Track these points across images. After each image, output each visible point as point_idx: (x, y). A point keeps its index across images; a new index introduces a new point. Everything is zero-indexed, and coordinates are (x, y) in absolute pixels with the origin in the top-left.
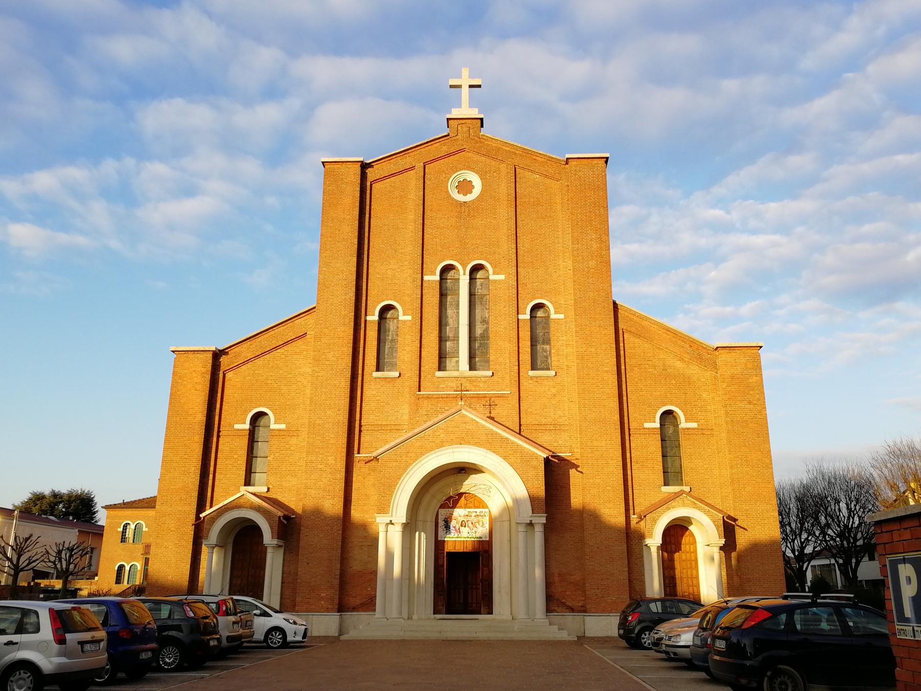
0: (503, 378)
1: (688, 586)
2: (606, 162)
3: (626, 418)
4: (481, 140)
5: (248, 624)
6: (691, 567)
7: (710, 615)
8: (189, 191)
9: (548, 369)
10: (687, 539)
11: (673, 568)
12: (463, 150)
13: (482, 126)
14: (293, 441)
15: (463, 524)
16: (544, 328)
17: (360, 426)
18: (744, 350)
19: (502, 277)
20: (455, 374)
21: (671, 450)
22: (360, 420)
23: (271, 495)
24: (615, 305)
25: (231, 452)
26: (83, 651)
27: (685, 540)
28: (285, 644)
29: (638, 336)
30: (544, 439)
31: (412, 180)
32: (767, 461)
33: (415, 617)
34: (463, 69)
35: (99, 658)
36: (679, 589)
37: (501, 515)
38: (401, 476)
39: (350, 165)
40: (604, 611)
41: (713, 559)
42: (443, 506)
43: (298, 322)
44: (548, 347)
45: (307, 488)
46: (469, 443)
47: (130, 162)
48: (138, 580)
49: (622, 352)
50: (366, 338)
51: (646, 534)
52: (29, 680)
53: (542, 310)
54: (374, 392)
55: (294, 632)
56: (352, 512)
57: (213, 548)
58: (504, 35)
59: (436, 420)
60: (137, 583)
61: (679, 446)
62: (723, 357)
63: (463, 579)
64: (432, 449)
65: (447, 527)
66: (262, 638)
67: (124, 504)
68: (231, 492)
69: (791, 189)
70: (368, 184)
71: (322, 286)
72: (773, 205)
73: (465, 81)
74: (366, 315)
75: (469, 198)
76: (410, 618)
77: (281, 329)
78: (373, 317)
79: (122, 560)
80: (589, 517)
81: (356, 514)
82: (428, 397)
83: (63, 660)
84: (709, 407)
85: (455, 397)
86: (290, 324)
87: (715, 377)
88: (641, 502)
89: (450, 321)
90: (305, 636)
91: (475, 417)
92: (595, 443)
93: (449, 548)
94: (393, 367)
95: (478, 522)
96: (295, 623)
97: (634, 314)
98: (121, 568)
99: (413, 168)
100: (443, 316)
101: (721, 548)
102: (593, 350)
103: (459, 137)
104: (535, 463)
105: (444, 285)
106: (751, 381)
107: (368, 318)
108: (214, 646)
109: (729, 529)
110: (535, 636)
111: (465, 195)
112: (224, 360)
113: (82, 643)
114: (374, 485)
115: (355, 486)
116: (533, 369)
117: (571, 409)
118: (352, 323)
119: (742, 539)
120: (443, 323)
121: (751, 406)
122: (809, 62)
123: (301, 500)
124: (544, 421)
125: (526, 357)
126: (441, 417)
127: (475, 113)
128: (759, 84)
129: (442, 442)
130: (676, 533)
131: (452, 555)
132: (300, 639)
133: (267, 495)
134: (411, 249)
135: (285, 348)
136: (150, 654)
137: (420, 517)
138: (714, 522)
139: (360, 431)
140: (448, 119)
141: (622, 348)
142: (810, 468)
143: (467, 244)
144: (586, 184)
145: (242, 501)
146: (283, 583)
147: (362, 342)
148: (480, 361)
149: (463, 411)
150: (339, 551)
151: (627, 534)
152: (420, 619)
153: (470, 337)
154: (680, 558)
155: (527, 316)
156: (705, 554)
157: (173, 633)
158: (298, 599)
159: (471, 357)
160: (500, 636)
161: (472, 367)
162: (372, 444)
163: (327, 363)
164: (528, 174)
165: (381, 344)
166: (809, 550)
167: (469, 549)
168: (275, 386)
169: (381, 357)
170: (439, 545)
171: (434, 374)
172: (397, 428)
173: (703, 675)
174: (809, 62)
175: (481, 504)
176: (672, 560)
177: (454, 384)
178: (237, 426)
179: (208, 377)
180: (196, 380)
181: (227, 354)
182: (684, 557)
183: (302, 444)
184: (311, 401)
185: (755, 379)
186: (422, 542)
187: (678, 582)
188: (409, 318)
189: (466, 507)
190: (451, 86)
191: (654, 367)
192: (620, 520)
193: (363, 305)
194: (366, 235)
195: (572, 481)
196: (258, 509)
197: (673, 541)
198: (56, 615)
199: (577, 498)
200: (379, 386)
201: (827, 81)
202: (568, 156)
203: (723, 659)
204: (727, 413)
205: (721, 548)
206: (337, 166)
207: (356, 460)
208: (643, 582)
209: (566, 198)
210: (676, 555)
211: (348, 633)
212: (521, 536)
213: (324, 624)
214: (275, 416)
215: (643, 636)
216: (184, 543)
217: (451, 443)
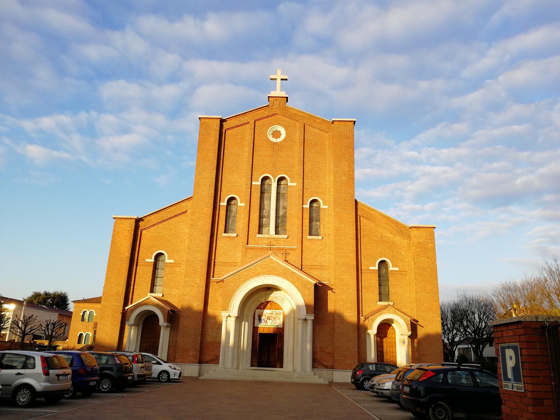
1: (390, 357)
2: (354, 124)
3: (360, 264)
4: (287, 109)
5: (149, 368)
6: (392, 346)
9: (318, 235)
12: (276, 114)
14: (178, 269)
15: (269, 318)
17: (215, 262)
19: (295, 184)
20: (267, 236)
23: (165, 298)
24: (356, 201)
26: (58, 380)
27: (390, 331)
28: (169, 380)
30: (315, 273)
33: (240, 368)
36: (385, 358)
37: (290, 314)
38: (236, 290)
39: (214, 120)
40: (344, 369)
42: (258, 308)
44: (318, 223)
45: (184, 295)
46: (274, 274)
47: (94, 114)
49: (359, 228)
50: (220, 215)
51: (369, 327)
53: (316, 203)
58: (301, 52)
60: (90, 344)
62: (414, 232)
63: (267, 348)
64: (253, 277)
65: (260, 320)
67: (84, 300)
68: (143, 296)
70: (224, 131)
71: (197, 185)
72: (444, 151)
73: (279, 76)
75: (279, 140)
76: (238, 368)
77: (173, 208)
78: (224, 204)
80: (337, 317)
81: (211, 310)
82: (252, 248)
83: (48, 384)
84: (405, 260)
85: (267, 249)
87: (409, 243)
88: (366, 309)
89: (266, 207)
90: (180, 376)
91: (277, 260)
93: (260, 331)
94: (234, 231)
96: (175, 369)
98: (81, 335)
99: (248, 123)
101: (409, 337)
102: (343, 226)
103: (274, 107)
104: (309, 286)
106: (429, 246)
107: (221, 204)
109: (414, 326)
110: (306, 381)
111: (276, 139)
112: (141, 223)
113: (58, 375)
114: (221, 295)
115: (210, 295)
119: (421, 332)
121: (428, 260)
122: (467, 73)
123: (181, 302)
124: (315, 264)
128: (439, 84)
132: (177, 377)
135: (175, 218)
136: (95, 383)
137: (245, 314)
138: (406, 322)
139: (214, 265)
140: (269, 97)
141: (359, 226)
142: (460, 294)
144: (342, 135)
145: (148, 301)
146: (169, 346)
148: (281, 230)
149: (271, 257)
156: (400, 340)
157: (108, 372)
158: (177, 356)
159: (277, 227)
161: (277, 233)
162: (220, 273)
164: (311, 128)
166: (457, 339)
167: (271, 332)
171: (256, 236)
172: (235, 265)
173: (396, 405)
174: (467, 73)
175: (279, 308)
176: (382, 342)
177: (266, 242)
178: (147, 260)
179: (132, 233)
180: (126, 234)
181: (143, 220)
186: (246, 327)
188: (243, 204)
189: (270, 309)
190: (271, 79)
192: (354, 319)
193: (219, 196)
194: (222, 158)
196: (157, 306)
197: (383, 332)
198: (45, 360)
199: (331, 306)
201: (476, 84)
202: (333, 119)
204: (415, 263)
205: (409, 337)
207: (211, 281)
208: (365, 354)
209: (331, 142)
210: (384, 340)
216: (116, 323)
217: (264, 273)
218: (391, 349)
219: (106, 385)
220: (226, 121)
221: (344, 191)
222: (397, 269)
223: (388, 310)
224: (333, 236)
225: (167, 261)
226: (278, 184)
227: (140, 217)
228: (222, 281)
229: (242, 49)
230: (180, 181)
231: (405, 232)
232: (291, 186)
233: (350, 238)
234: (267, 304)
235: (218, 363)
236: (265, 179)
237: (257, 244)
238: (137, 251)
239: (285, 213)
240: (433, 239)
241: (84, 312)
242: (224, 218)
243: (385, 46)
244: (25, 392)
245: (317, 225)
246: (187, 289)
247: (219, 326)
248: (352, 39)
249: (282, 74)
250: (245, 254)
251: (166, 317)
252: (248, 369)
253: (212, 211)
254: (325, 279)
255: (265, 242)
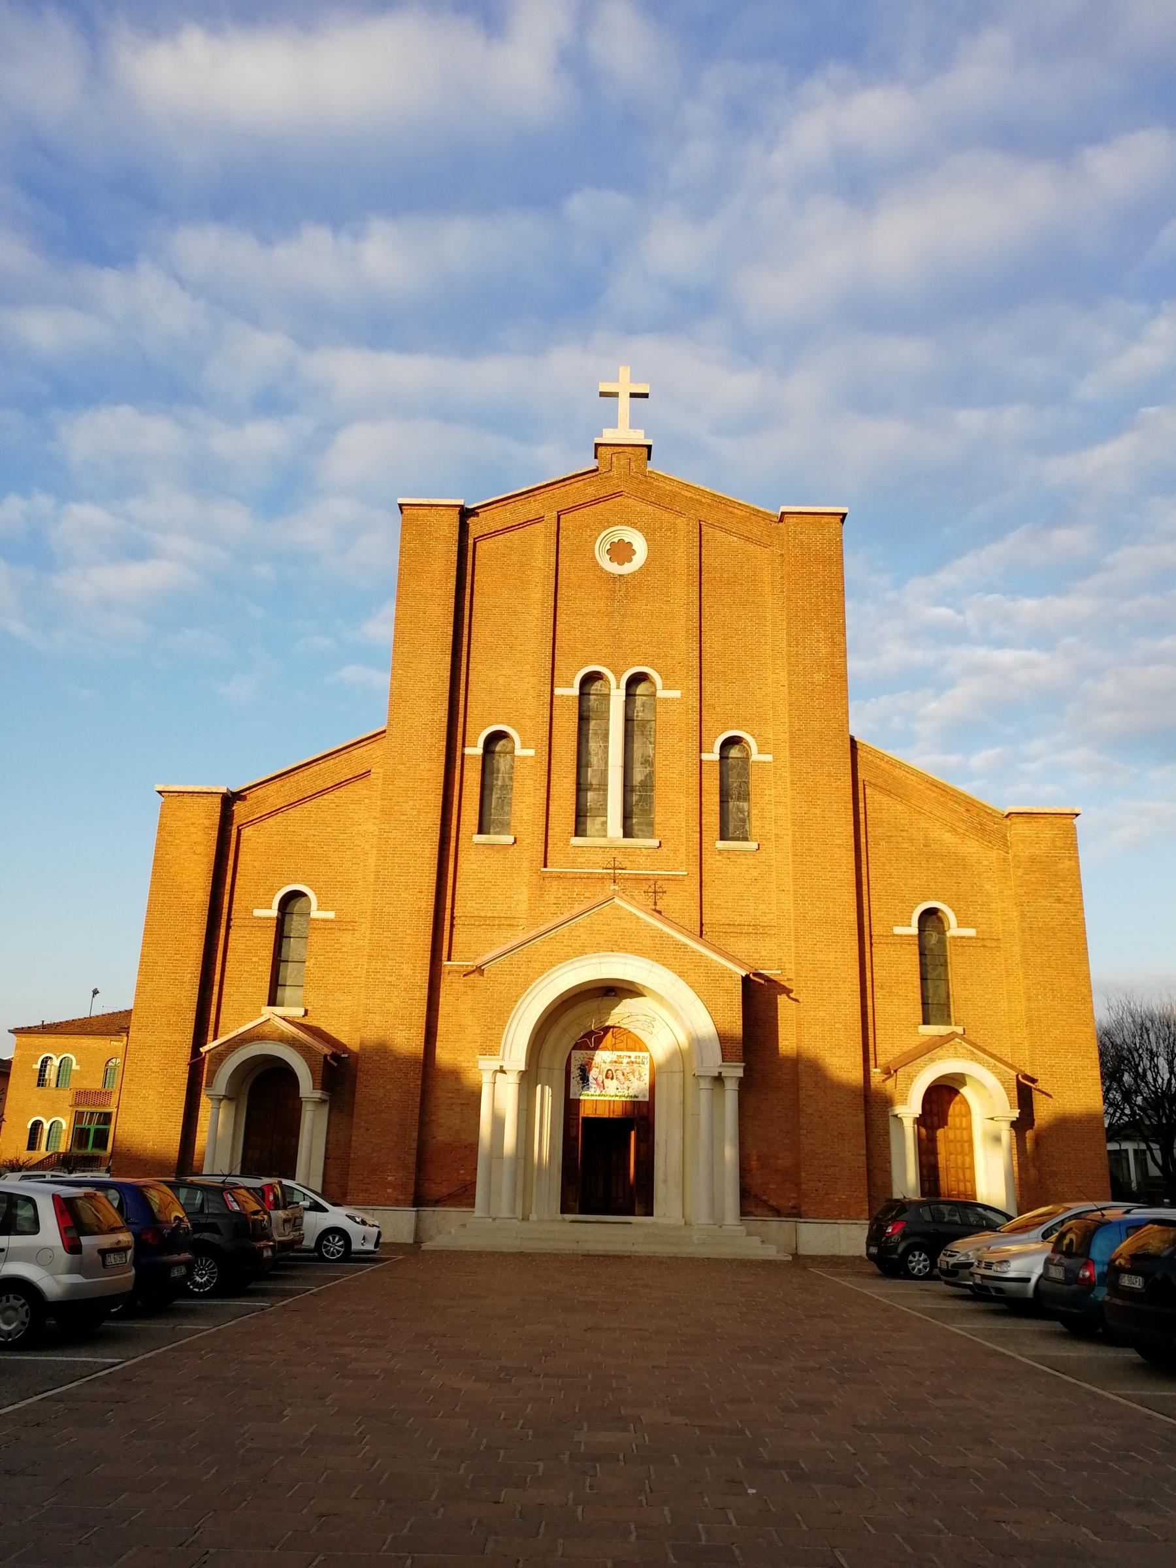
0: (676, 851)
1: (958, 1181)
2: (842, 521)
3: (866, 919)
4: (648, 479)
5: (295, 1222)
6: (962, 1152)
7: (1070, 1236)
8: (136, 551)
9: (746, 839)
10: (957, 1107)
11: (934, 1153)
12: (619, 494)
13: (649, 459)
14: (346, 938)
15: (609, 1075)
16: (739, 775)
17: (453, 918)
18: (1051, 819)
19: (677, 694)
20: (601, 842)
21: (934, 970)
22: (453, 908)
23: (310, 1021)
24: (852, 740)
25: (248, 954)
26: (104, 1265)
27: (954, 1109)
28: (348, 1255)
29: (887, 792)
30: (741, 946)
31: (540, 538)
32: (1085, 991)
33: (533, 1217)
34: (621, 368)
35: (125, 1276)
36: (943, 1184)
37: (669, 1061)
38: (518, 997)
39: (443, 511)
40: (827, 1216)
41: (997, 1139)
42: (577, 1047)
43: (356, 752)
44: (746, 805)
45: (368, 1011)
46: (626, 950)
47: (44, 502)
48: (64, 1145)
49: (862, 816)
50: (466, 785)
51: (897, 1097)
52: (23, 1311)
53: (737, 747)
54: (473, 866)
55: (361, 1238)
56: (438, 1051)
57: (220, 1100)
58: (631, 328)
59: (574, 912)
60: (62, 1149)
61: (945, 965)
62: (1020, 829)
63: (606, 1160)
64: (567, 958)
65: (584, 1079)
66: (313, 1245)
67: (43, 1026)
68: (245, 1013)
69: (1055, 579)
70: (471, 541)
71: (397, 698)
72: (1029, 604)
73: (624, 385)
74: (464, 746)
75: (627, 569)
76: (525, 1218)
77: (331, 762)
78: (475, 750)
79: (39, 1114)
80: (805, 1069)
81: (444, 1055)
82: (559, 877)
83: (77, 1279)
84: (994, 906)
85: (601, 878)
86: (344, 756)
87: (1005, 860)
88: (887, 1048)
89: (594, 760)
90: (377, 1245)
91: (632, 908)
92: (819, 956)
93: (586, 1111)
94: (504, 827)
95: (633, 1073)
96: (364, 1223)
97: (883, 757)
98: (37, 1125)
99: (540, 519)
100: (584, 752)
101: (1013, 1124)
102: (818, 811)
103: (614, 473)
104: (727, 984)
105: (585, 704)
106: (1061, 866)
107: (468, 751)
108: (268, 1258)
109: (1025, 1094)
110: (726, 1252)
111: (621, 563)
112: (238, 807)
113: (103, 1252)
114: (473, 1010)
115: (442, 1010)
116: (723, 838)
117: (781, 898)
118: (443, 758)
119: (1044, 1111)
120: (584, 762)
121: (1060, 906)
122: (1089, 390)
123: (358, 1030)
124: (739, 920)
125: (712, 819)
126: (582, 908)
127: (638, 437)
128: (1012, 419)
129: (584, 946)
130: (943, 1095)
131: (595, 1125)
132: (372, 1248)
133: (303, 1021)
134: (535, 646)
135: (337, 793)
136: (183, 1270)
137: (544, 1062)
138: (1003, 1083)
139: (452, 926)
140: (597, 445)
141: (862, 810)
142: (1114, 1003)
143: (623, 640)
144: (811, 554)
145: (266, 1029)
146: (326, 1158)
147: (457, 787)
148: (639, 824)
149: (617, 901)
150: (417, 1111)
151: (865, 1096)
152: (540, 1221)
153: (625, 786)
154: (946, 1137)
155: (715, 756)
156: (985, 1134)
157: (206, 1236)
158: (351, 1185)
159: (627, 816)
160: (672, 1250)
161: (627, 833)
162: (467, 948)
163: (403, 818)
164: (719, 534)
165: (486, 792)
167: (618, 1113)
168: (319, 851)
169: (486, 813)
170: (571, 1106)
171: (568, 840)
172: (509, 923)
173: (1057, 1326)
174: (1089, 390)
175: (637, 1045)
176: (933, 1140)
177: (598, 858)
178: (257, 913)
179: (215, 834)
180: (194, 838)
181: (244, 798)
182: (951, 1136)
183: (361, 943)
184: (377, 878)
185: (1067, 864)
186: (546, 1099)
187: (942, 1174)
188: (531, 752)
189: (614, 1048)
190: (602, 394)
191: (911, 840)
192: (856, 1076)
193: (460, 730)
194: (466, 621)
195: (782, 1013)
196: (292, 1042)
197: (935, 1110)
198: (65, 1207)
199: (788, 1040)
200: (482, 857)
201: (1114, 419)
202: (784, 509)
203: (1128, 1303)
204: (1023, 915)
205: (1013, 1124)
206: (422, 512)
207: (445, 970)
208: (888, 1173)
209: (779, 574)
210: (940, 1133)
211: (431, 1238)
212: (704, 1096)
213: (397, 1223)
214: (318, 899)
215: (911, 1258)
216: (172, 1091)
217: (598, 948)
218: (960, 1158)
219: (202, 1276)
220: (477, 514)
221: (818, 713)
222: (971, 932)
223: (951, 1050)
224: (788, 840)
225: (315, 914)
226: (628, 695)
227: (235, 790)
228: (479, 970)
229: (464, 319)
230: (361, 679)
231: (991, 826)
232: (666, 700)
233: (839, 846)
234: (605, 1034)
235: (472, 1205)
236: (590, 679)
237: (573, 864)
238: (228, 887)
239: (650, 776)
240: (1072, 846)
241: (45, 1062)
242: (478, 790)
243: (868, 312)
244: (13, 1302)
245: (741, 810)
246: (378, 995)
247: (473, 1099)
248: (776, 291)
249: (633, 380)
250: (539, 892)
251: (320, 1073)
252: (554, 1221)
253: (443, 772)
254: (769, 964)
255: (593, 857)
